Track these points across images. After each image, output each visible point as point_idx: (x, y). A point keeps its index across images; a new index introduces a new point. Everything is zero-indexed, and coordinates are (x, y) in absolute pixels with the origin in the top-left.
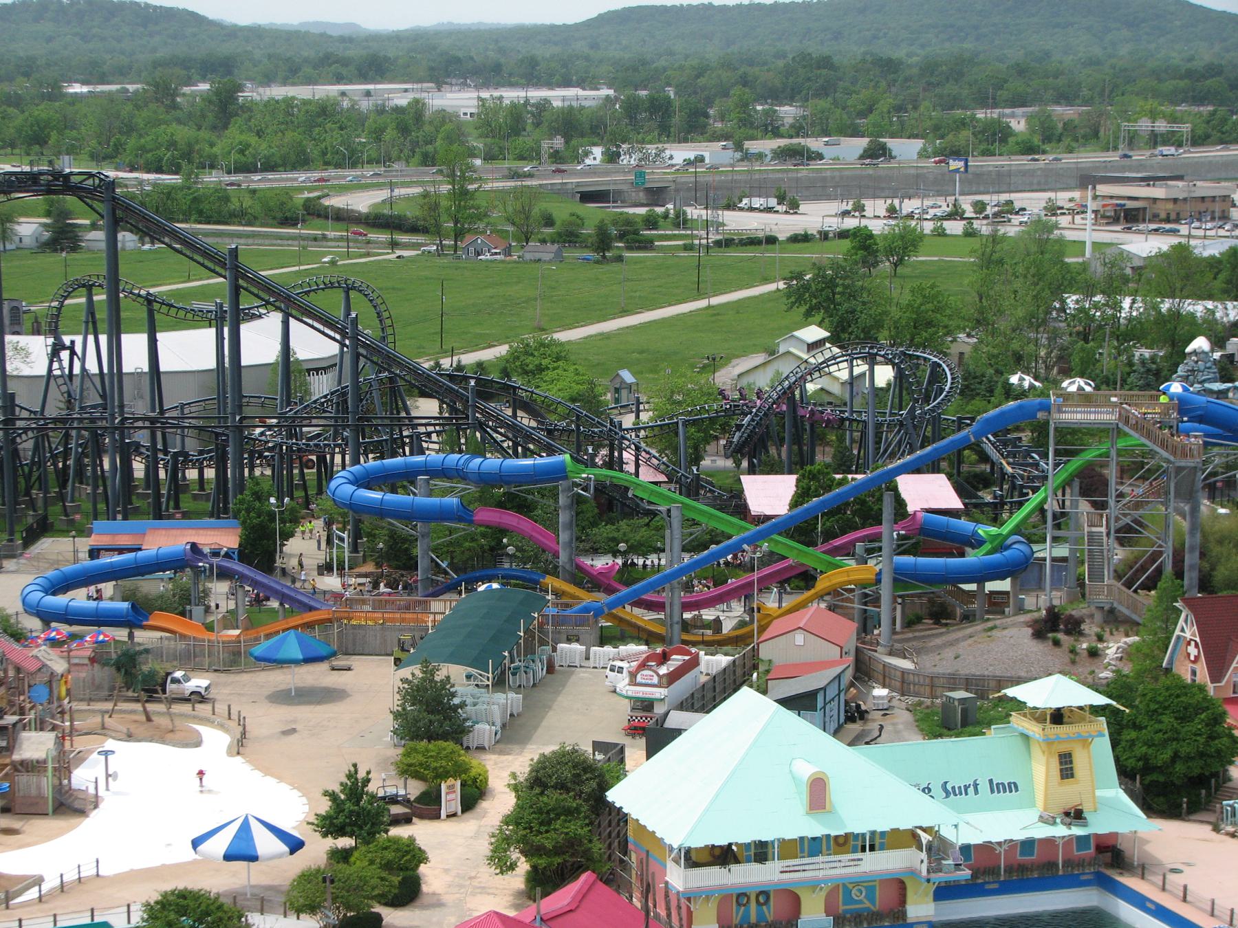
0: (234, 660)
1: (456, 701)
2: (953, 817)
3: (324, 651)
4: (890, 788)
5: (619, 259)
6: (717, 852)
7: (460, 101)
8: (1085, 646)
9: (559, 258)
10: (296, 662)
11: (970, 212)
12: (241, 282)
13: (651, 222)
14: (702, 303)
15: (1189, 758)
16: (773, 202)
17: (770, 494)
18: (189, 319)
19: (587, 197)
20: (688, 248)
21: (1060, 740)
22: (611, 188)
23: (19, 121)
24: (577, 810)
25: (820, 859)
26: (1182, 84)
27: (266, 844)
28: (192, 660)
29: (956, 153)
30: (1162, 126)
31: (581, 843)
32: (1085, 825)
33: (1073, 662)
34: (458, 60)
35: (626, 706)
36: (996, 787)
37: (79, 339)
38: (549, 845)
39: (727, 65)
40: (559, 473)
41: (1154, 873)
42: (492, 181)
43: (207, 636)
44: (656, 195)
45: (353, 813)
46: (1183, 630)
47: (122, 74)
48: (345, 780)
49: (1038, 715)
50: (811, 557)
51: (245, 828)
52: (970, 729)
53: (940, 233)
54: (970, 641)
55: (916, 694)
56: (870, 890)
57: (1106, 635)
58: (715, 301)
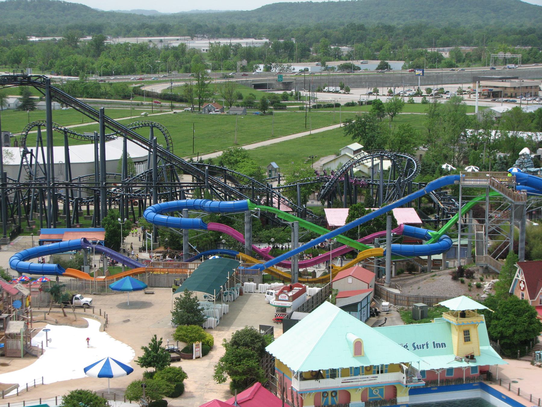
0: (102, 289)
1: (200, 307)
2: (417, 359)
3: (142, 285)
4: (390, 346)
5: (271, 114)
6: (314, 374)
7: (202, 44)
8: (475, 283)
9: (245, 113)
10: (130, 290)
11: (424, 93)
12: (105, 124)
13: (285, 97)
14: (308, 133)
15: (520, 332)
16: (338, 89)
17: (337, 217)
18: (83, 140)
19: (257, 86)
20: (301, 109)
21: (464, 325)
22: (268, 82)
23: (8, 53)
24: (253, 355)
25: (359, 377)
26: (517, 37)
27: (116, 370)
28: (84, 289)
29: (419, 67)
30: (509, 55)
31: (254, 370)
32: (475, 362)
33: (470, 290)
34: (201, 26)
35: (274, 310)
36: (436, 345)
37: (34, 149)
38: (240, 371)
39: (318, 28)
40: (245, 208)
41: (505, 383)
42: (215, 79)
43: (91, 279)
44: (287, 85)
45: (155, 356)
46: (518, 276)
47: (53, 33)
48: (151, 342)
49: (454, 314)
50: (355, 244)
51: (107, 363)
52: (425, 320)
53: (412, 102)
54: (425, 281)
55: (401, 305)
56: (381, 390)
57: (484, 279)
58: (313, 132)
